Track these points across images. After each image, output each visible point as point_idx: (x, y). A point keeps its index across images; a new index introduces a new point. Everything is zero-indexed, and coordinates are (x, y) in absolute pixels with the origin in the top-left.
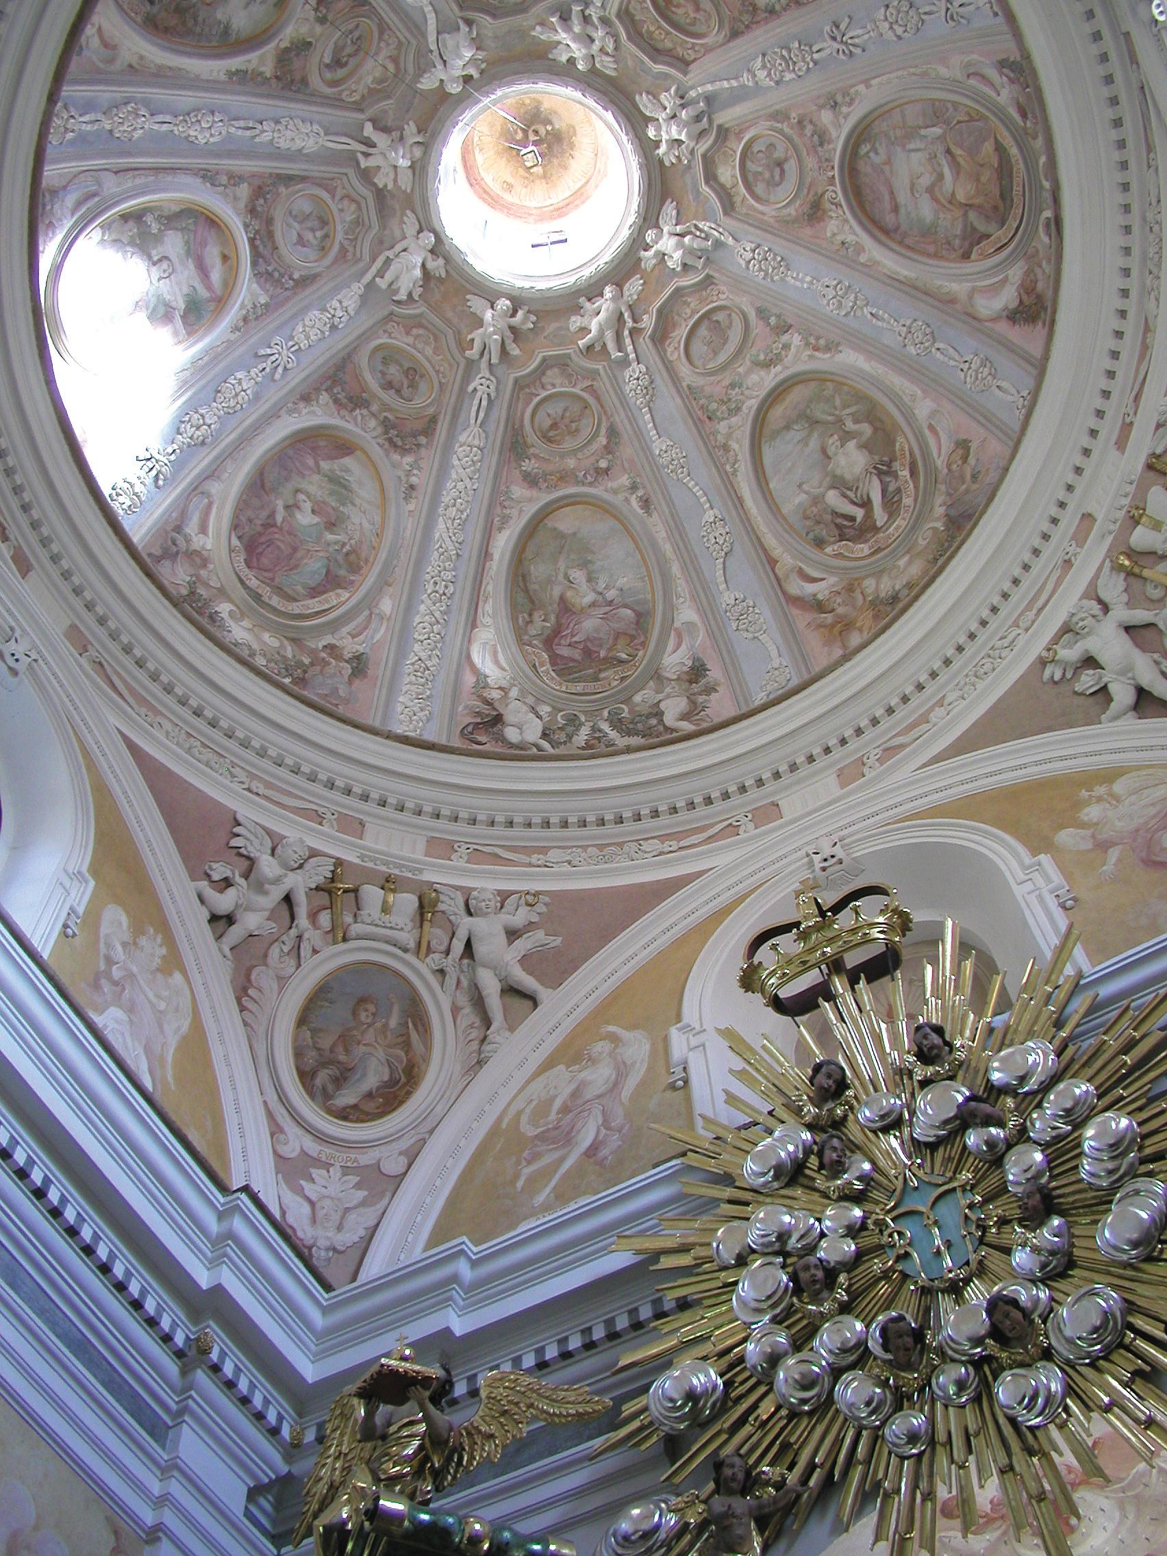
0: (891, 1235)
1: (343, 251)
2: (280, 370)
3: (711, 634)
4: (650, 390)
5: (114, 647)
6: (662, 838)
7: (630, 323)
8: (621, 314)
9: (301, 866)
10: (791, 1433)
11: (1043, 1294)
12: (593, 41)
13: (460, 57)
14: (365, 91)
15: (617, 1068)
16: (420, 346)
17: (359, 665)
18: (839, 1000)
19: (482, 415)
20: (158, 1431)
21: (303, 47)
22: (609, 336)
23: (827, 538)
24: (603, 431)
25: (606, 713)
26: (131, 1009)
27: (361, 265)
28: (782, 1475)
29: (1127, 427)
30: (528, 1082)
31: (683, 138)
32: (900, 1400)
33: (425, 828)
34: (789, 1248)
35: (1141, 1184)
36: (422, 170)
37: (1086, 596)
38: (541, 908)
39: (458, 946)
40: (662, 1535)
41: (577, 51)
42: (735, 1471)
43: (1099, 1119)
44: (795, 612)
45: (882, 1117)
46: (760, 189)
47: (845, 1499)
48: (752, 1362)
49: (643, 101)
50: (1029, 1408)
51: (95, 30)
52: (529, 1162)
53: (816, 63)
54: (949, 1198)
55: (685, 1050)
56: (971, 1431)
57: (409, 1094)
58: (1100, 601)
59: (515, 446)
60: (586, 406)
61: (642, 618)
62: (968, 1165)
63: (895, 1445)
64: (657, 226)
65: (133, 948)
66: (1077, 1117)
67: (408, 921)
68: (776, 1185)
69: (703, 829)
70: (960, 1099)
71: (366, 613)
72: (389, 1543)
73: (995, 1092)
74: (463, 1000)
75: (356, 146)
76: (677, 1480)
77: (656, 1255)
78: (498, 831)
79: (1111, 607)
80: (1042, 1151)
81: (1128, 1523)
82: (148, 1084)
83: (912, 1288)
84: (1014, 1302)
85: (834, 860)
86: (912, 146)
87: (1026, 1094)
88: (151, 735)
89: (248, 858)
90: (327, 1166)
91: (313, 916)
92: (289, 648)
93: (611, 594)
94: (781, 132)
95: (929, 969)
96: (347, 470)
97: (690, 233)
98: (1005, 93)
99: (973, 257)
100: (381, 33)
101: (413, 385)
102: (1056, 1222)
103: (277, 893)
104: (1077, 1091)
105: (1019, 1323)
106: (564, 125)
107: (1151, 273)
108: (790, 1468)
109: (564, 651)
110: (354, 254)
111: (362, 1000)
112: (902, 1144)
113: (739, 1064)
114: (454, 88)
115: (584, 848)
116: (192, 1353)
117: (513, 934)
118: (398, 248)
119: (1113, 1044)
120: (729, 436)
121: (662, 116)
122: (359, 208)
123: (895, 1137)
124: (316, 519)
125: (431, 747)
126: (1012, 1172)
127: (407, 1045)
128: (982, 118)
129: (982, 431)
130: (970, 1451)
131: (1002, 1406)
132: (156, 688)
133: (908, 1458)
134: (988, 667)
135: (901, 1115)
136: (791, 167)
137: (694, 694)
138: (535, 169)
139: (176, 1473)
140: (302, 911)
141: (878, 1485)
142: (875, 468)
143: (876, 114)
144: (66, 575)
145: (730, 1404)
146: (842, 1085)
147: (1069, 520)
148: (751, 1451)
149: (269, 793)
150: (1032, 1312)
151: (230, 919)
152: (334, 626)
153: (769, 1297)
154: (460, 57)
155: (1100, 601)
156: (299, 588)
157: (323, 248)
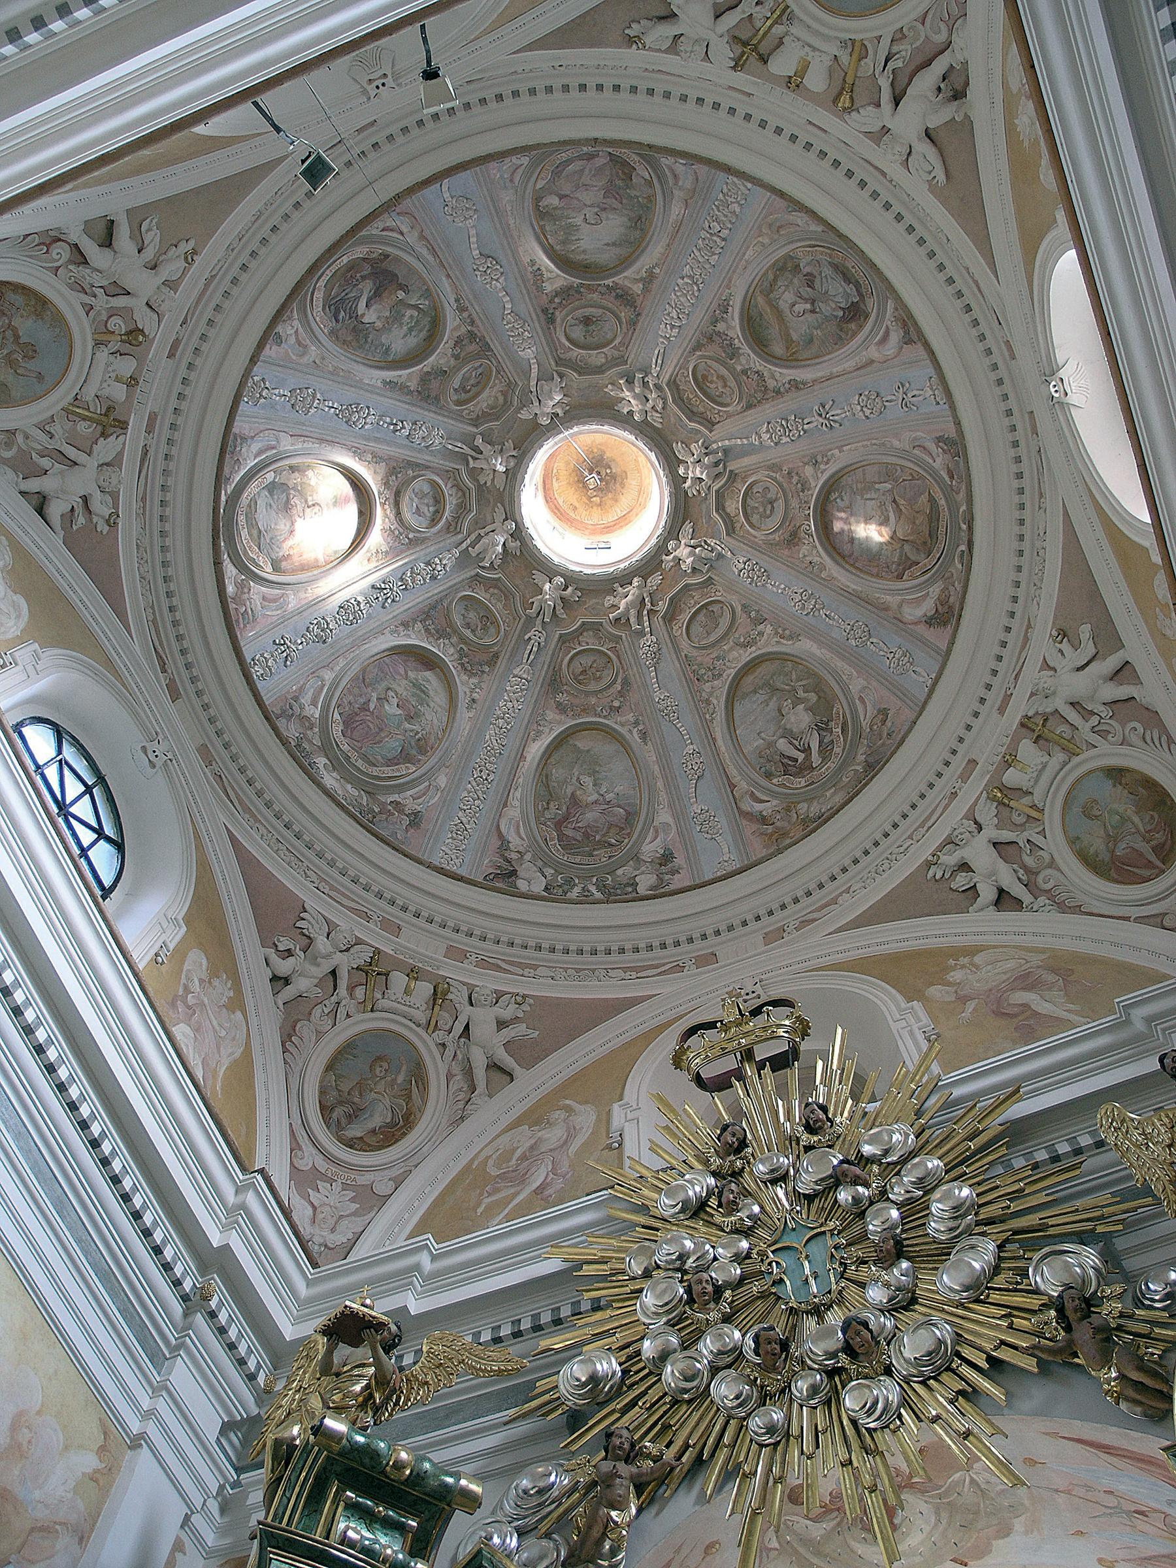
0: (770, 1264)
1: (448, 525)
2: (389, 601)
3: (680, 833)
4: (657, 655)
5: (233, 767)
6: (625, 970)
7: (649, 606)
8: (644, 599)
9: (347, 950)
10: (671, 1417)
11: (889, 1324)
12: (648, 400)
13: (552, 399)
14: (480, 413)
15: (568, 1130)
16: (494, 602)
17: (415, 819)
18: (748, 1081)
19: (532, 657)
20: (156, 1358)
21: (442, 373)
22: (633, 612)
23: (775, 773)
24: (619, 681)
25: (594, 880)
26: (197, 1029)
27: (460, 536)
28: (661, 1451)
29: (1008, 697)
30: (498, 1136)
31: (704, 477)
32: (764, 1398)
33: (447, 939)
34: (686, 1267)
35: (974, 1240)
36: (514, 476)
37: (966, 817)
38: (526, 1007)
39: (459, 1028)
40: (555, 1493)
41: (636, 406)
42: (622, 1440)
43: (944, 1187)
44: (745, 822)
45: (772, 1171)
46: (755, 518)
47: (710, 1476)
48: (647, 1356)
49: (678, 448)
50: (869, 1413)
51: (293, 331)
52: (490, 1195)
53: (805, 432)
54: (819, 1238)
55: (623, 1121)
56: (820, 1428)
57: (405, 1134)
58: (976, 822)
59: (554, 683)
60: (610, 660)
61: (631, 816)
62: (837, 1215)
63: (756, 1433)
64: (681, 462)
65: (207, 984)
66: (927, 1185)
67: (423, 1003)
68: (682, 1217)
69: (656, 967)
70: (835, 1162)
71: (427, 784)
72: (328, 1457)
73: (864, 1161)
74: (456, 1069)
75: (467, 450)
76: (574, 1448)
77: (579, 1266)
78: (502, 948)
79: (983, 827)
80: (898, 1209)
81: (941, 1528)
82: (199, 1074)
83: (783, 1307)
84: (865, 1324)
85: (754, 995)
86: (868, 496)
87: (889, 1164)
88: (251, 836)
89: (309, 937)
90: (331, 1181)
91: (351, 989)
92: (365, 798)
93: (609, 797)
94: (775, 479)
95: (820, 1064)
96: (428, 681)
97: (701, 546)
98: (939, 460)
99: (904, 578)
100: (498, 372)
101: (485, 628)
102: (905, 1265)
103: (327, 967)
104: (930, 1165)
105: (867, 1342)
106: (619, 470)
107: (1035, 585)
108: (668, 1446)
109: (570, 833)
110: (456, 528)
111: (379, 1058)
112: (786, 1194)
113: (664, 1121)
114: (545, 421)
115: (566, 969)
116: (195, 1299)
117: (501, 1024)
118: (488, 529)
119: (962, 1133)
120: (711, 694)
121: (690, 460)
122: (464, 495)
123: (781, 1187)
124: (400, 712)
125: (460, 879)
126: (874, 1226)
127: (408, 1097)
128: (922, 477)
129: (899, 702)
130: (818, 1447)
131: (847, 1410)
132: (260, 803)
133: (767, 1446)
134: (885, 867)
135: (788, 1171)
136: (780, 505)
137: (662, 874)
138: (594, 499)
139: (164, 1393)
140: (343, 983)
141: (738, 1466)
142: (816, 725)
143: (846, 470)
144: (206, 707)
145: (625, 1389)
146: (743, 1144)
147: (958, 763)
148: (638, 1428)
149: (332, 893)
150: (879, 1335)
151: (287, 981)
152: (401, 788)
153: (667, 1304)
154: (552, 399)
155: (976, 822)
156: (379, 757)
157: (433, 520)
